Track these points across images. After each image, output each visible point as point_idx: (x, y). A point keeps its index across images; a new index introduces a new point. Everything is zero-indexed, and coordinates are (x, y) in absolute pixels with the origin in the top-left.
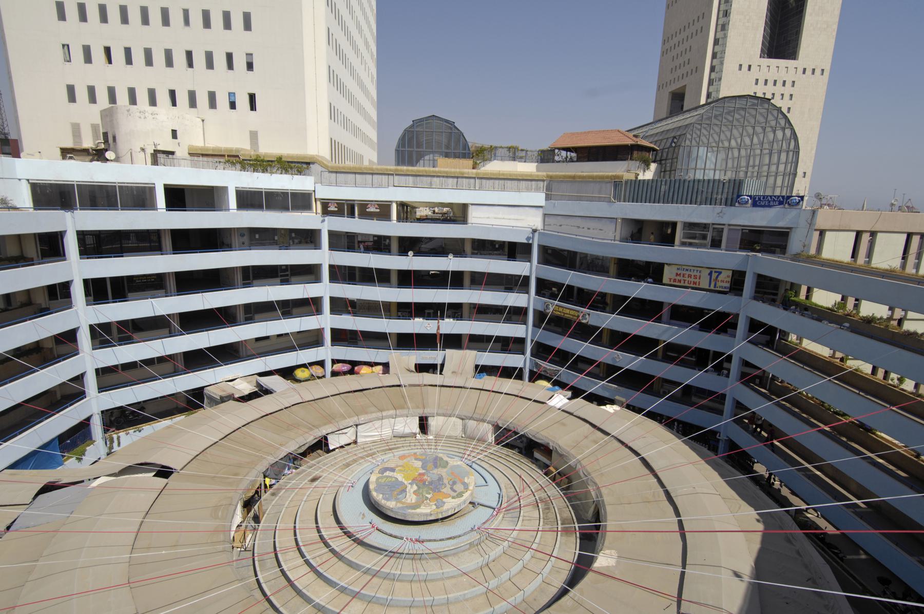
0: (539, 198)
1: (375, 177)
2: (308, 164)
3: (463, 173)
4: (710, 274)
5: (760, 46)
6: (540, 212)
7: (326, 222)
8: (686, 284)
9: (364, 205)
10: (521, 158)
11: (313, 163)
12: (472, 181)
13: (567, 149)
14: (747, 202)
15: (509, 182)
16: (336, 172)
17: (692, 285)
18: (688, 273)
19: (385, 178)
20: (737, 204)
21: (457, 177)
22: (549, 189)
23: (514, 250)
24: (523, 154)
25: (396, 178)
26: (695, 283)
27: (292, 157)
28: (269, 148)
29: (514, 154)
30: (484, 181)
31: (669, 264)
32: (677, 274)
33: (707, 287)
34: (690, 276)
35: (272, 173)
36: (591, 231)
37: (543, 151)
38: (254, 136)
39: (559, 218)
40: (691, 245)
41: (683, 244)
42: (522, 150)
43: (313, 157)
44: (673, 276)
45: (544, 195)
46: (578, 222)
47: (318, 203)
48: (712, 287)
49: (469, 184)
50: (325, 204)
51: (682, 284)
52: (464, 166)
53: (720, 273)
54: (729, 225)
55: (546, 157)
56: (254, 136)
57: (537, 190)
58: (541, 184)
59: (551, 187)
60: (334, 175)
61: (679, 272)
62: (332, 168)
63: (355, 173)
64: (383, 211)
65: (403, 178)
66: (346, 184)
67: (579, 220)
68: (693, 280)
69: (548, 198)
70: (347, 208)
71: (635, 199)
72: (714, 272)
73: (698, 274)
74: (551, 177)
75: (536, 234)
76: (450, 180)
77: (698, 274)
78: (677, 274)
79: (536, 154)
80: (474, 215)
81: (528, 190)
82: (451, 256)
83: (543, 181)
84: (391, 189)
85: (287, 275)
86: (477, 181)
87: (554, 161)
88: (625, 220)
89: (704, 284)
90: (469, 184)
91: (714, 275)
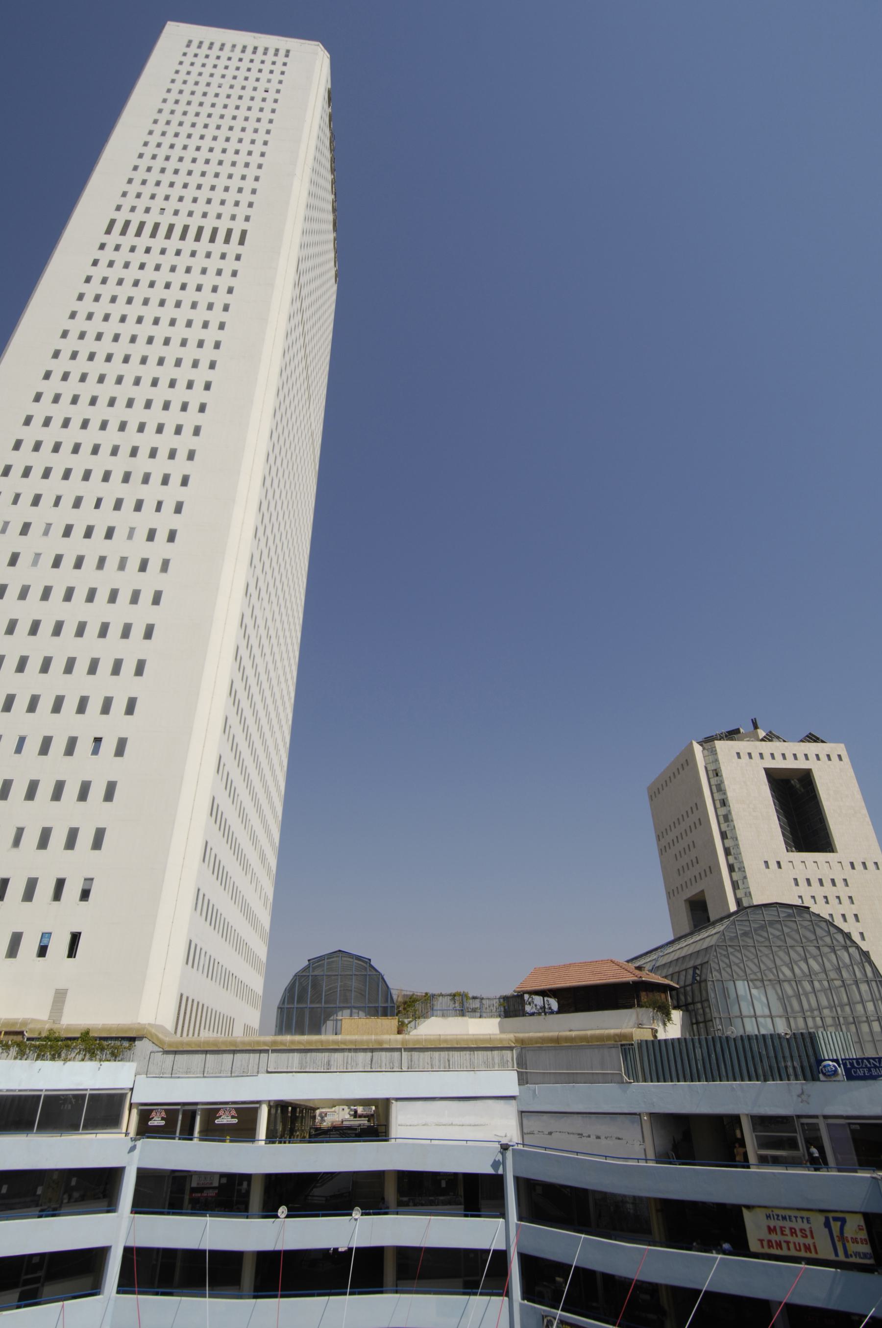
0: (506, 1081)
1: (238, 1056)
2: (132, 1039)
3: (380, 1042)
4: (827, 1224)
5: (781, 838)
6: (510, 1111)
7: (137, 1152)
8: (793, 1253)
9: (212, 1111)
10: (474, 1010)
11: (141, 1038)
12: (396, 1055)
13: (543, 993)
14: (835, 1072)
15: (456, 1054)
16: (176, 1052)
17: (803, 1254)
18: (787, 1224)
19: (254, 1057)
20: (821, 1076)
21: (372, 1050)
22: (521, 1063)
23: (471, 1193)
24: (476, 1004)
25: (273, 1056)
26: (807, 1248)
27: (110, 1030)
28: (77, 1017)
29: (463, 1005)
30: (415, 1054)
31: (748, 1207)
32: (771, 1230)
33: (832, 1257)
34: (793, 1232)
35: (65, 1060)
36: (603, 1141)
37: (506, 998)
38: (60, 997)
39: (545, 1117)
40: (776, 1161)
41: (763, 1160)
42: (474, 998)
43: (143, 1027)
44: (765, 1235)
45: (514, 1075)
46: (578, 1124)
47: (135, 1112)
48: (842, 1257)
49: (392, 1061)
50: (145, 1113)
51: (784, 1252)
52: (383, 1030)
53: (843, 1221)
54: (826, 1117)
55: (512, 1006)
56: (60, 997)
57: (503, 1066)
58: (508, 1054)
59: (527, 1060)
60: (171, 1057)
61: (772, 1223)
62: (170, 1045)
63: (206, 1052)
64: (242, 1123)
65: (284, 1056)
66: (188, 1073)
67: (579, 1120)
68: (800, 1240)
69: (523, 1080)
70: (179, 1121)
71: (660, 1076)
72: (833, 1218)
73: (806, 1226)
74: (522, 1041)
75: (509, 1154)
76: (361, 1056)
77: (806, 1226)
78: (771, 1230)
79: (496, 1003)
80: (402, 1121)
81: (489, 1066)
82: (357, 1213)
83: (511, 1048)
84: (263, 1076)
85: (36, 1280)
86: (404, 1054)
87: (524, 1014)
88: (652, 1115)
89: (825, 1251)
90: (392, 1061)
91: (836, 1226)
